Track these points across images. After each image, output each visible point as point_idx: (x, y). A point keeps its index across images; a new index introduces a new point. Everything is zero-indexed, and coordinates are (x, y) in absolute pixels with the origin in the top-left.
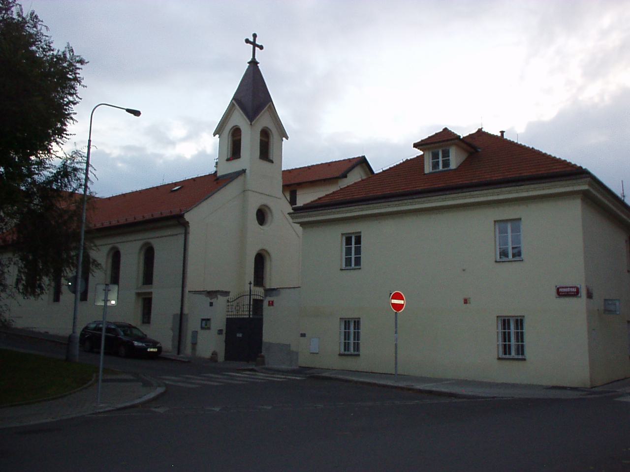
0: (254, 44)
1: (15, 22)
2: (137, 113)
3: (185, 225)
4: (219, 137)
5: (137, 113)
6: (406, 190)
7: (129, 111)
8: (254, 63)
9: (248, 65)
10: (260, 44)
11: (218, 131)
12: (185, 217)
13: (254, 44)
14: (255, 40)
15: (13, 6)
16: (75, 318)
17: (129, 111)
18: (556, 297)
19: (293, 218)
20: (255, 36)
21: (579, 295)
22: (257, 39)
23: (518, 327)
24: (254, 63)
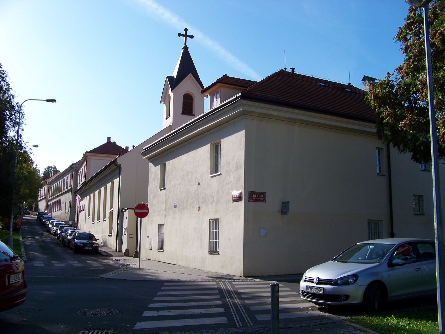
0: (186, 36)
2: (53, 101)
5: (53, 101)
7: (47, 101)
8: (186, 49)
14: (186, 33)
17: (47, 101)
18: (248, 201)
24: (186, 49)
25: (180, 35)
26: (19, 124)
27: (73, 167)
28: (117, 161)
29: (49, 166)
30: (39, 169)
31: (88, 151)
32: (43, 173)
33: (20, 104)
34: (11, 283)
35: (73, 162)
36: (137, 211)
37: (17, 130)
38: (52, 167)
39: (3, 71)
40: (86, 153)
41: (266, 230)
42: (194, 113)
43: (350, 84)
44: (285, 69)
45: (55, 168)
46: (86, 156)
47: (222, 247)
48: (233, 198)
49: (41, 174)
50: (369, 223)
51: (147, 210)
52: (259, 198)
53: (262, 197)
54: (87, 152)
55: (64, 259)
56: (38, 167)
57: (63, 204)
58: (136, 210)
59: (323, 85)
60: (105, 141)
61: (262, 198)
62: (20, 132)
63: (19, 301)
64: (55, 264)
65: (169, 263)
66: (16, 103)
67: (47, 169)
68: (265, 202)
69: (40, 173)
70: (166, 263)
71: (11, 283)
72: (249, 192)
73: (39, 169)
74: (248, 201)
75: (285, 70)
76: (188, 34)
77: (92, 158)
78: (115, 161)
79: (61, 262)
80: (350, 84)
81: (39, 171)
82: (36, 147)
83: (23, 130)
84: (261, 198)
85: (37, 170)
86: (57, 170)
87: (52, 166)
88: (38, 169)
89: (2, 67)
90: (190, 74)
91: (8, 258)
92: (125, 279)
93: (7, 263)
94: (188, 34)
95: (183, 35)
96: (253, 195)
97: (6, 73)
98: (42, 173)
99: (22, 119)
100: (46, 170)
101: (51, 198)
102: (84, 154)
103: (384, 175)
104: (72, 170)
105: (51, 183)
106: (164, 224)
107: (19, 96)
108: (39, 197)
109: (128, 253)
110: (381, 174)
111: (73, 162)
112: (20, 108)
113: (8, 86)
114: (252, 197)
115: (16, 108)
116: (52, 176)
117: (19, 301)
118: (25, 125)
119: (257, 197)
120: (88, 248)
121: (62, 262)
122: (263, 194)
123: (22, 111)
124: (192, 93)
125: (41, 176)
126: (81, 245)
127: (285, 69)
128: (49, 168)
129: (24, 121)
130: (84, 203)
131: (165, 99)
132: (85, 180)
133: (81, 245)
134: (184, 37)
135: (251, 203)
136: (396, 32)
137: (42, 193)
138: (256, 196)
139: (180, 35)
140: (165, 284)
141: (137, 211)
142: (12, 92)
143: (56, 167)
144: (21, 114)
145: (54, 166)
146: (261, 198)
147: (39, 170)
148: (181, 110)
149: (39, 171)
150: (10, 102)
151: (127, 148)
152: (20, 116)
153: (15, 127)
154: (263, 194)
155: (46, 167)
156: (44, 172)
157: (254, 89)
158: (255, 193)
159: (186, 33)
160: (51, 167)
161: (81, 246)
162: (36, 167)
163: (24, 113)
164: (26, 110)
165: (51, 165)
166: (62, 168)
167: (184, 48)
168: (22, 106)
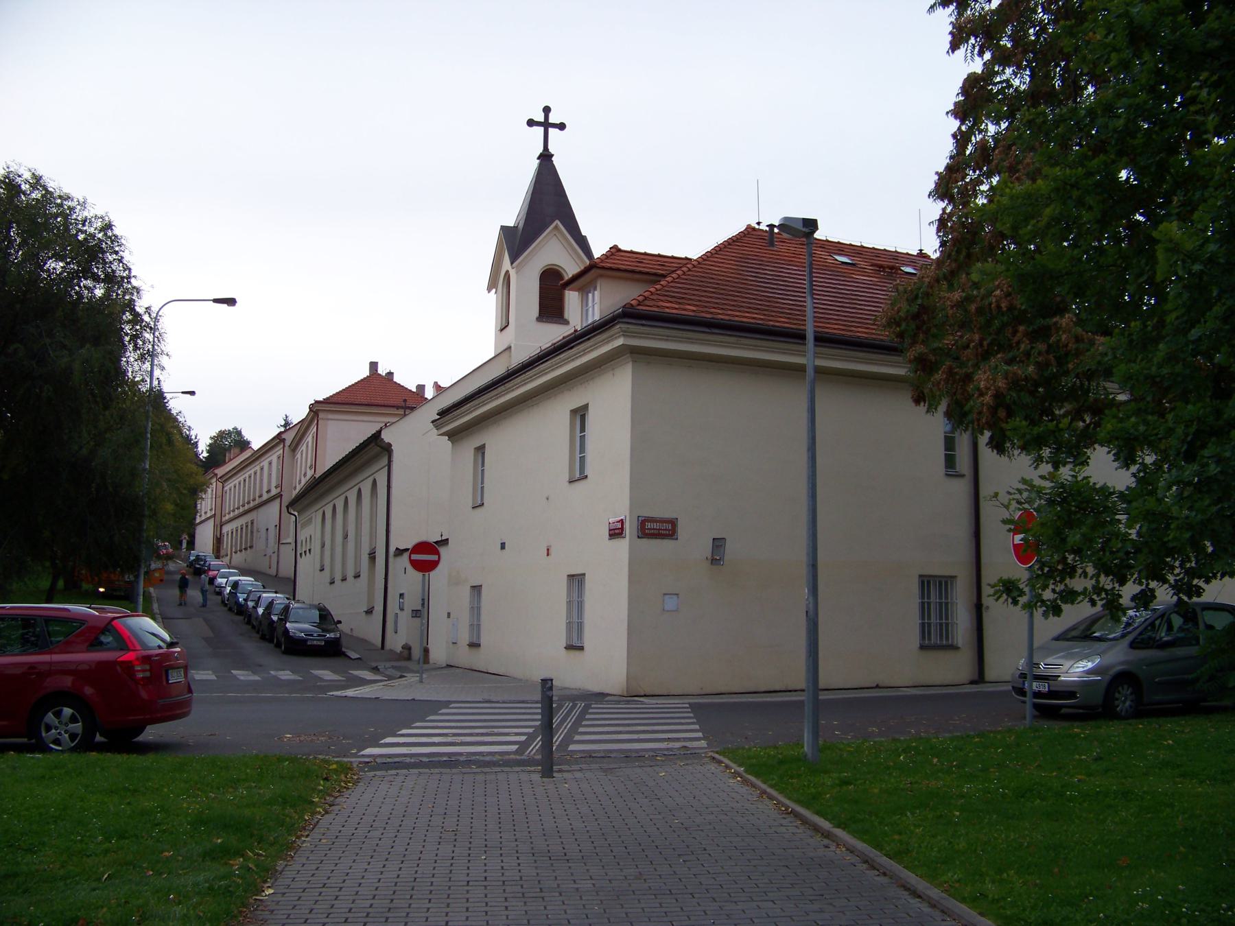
0: (546, 125)
1: (1009, 67)
2: (231, 302)
3: (387, 449)
4: (496, 293)
5: (231, 302)
6: (772, 323)
7: (217, 301)
8: (546, 157)
9: (538, 161)
10: (535, 128)
11: (492, 285)
12: (382, 437)
13: (546, 125)
14: (547, 117)
15: (976, 41)
16: (915, 687)
17: (217, 301)
18: (638, 537)
19: (437, 427)
20: (547, 110)
21: (675, 537)
22: (551, 115)
23: (925, 638)
24: (546, 157)
25: (531, 123)
26: (152, 354)
27: (284, 439)
30: (196, 438)
31: (321, 399)
32: (208, 448)
33: (155, 309)
34: (170, 682)
36: (414, 557)
37: (149, 369)
39: (116, 236)
40: (317, 405)
41: (678, 597)
42: (566, 316)
43: (921, 250)
44: (759, 223)
45: (239, 433)
46: (317, 409)
48: (610, 530)
49: (200, 452)
50: (923, 582)
51: (437, 556)
52: (661, 529)
53: (670, 528)
54: (317, 402)
55: (261, 666)
56: (193, 433)
58: (412, 555)
59: (843, 263)
60: (365, 373)
61: (669, 530)
62: (157, 373)
63: (231, 570)
64: (238, 677)
65: (490, 673)
66: (146, 308)
68: (677, 539)
69: (200, 449)
70: (485, 673)
71: (170, 682)
72: (640, 519)
73: (196, 438)
74: (638, 537)
75: (757, 227)
77: (330, 416)
78: (376, 436)
79: (253, 672)
80: (921, 250)
81: (197, 442)
82: (189, 395)
83: (163, 369)
84: (666, 530)
85: (192, 440)
86: (245, 439)
88: (193, 437)
89: (113, 227)
91: (162, 644)
92: (376, 698)
93: (161, 651)
95: (538, 124)
96: (648, 525)
97: (123, 241)
98: (205, 450)
99: (159, 344)
100: (215, 441)
101: (227, 517)
102: (310, 408)
103: (963, 476)
104: (282, 446)
105: (224, 479)
106: (481, 586)
107: (150, 289)
108: (199, 514)
109: (410, 654)
110: (957, 474)
112: (156, 318)
113: (127, 272)
114: (648, 529)
115: (146, 318)
116: (231, 460)
117: (231, 570)
118: (168, 357)
119: (659, 529)
121: (254, 673)
122: (673, 523)
123: (159, 327)
124: (562, 268)
125: (201, 457)
127: (759, 223)
128: (222, 435)
129: (164, 349)
130: (311, 531)
131: (500, 281)
132: (315, 472)
134: (542, 128)
135: (644, 540)
136: (930, 183)
137: (206, 505)
138: (655, 527)
139: (531, 123)
140: (452, 705)
141: (414, 557)
142: (134, 282)
143: (240, 431)
144: (157, 334)
145: (237, 429)
146: (666, 530)
147: (196, 440)
149: (197, 442)
150: (130, 306)
151: (421, 388)
152: (154, 337)
153: (144, 363)
154: (673, 523)
156: (210, 445)
157: (658, 292)
159: (547, 117)
163: (163, 331)
164: (165, 324)
166: (257, 439)
168: (160, 314)
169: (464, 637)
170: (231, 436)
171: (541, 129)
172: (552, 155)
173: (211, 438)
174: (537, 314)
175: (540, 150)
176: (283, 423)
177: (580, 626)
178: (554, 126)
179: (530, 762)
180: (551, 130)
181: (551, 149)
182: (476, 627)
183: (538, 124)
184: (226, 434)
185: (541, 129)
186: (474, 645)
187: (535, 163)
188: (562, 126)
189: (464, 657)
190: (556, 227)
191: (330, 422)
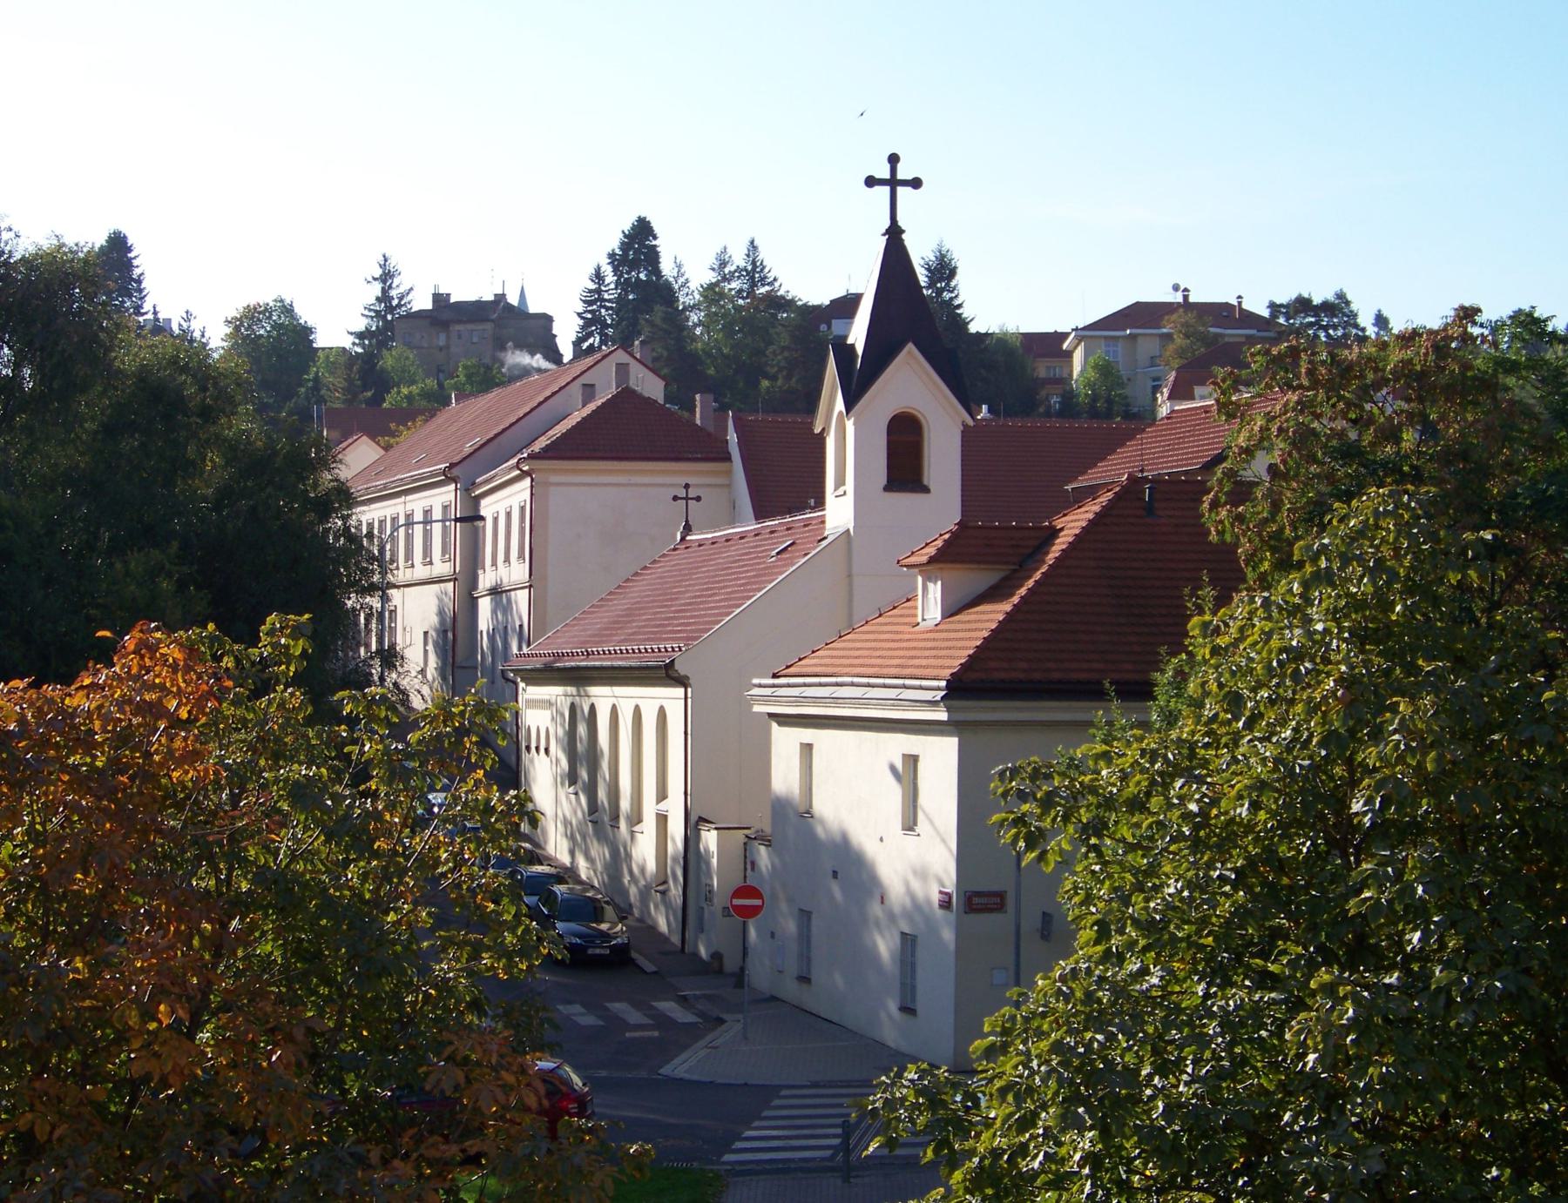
8: (894, 233)
10: (877, 188)
13: (893, 183)
14: (893, 171)
24: (894, 233)
25: (871, 182)
28: (677, 666)
29: (252, 303)
30: (203, 336)
35: (386, 260)
38: (267, 311)
42: (925, 482)
45: (288, 310)
47: (922, 1002)
57: (408, 635)
67: (240, 319)
73: (203, 336)
76: (902, 174)
77: (554, 479)
86: (302, 321)
87: (271, 304)
88: (197, 335)
90: (910, 347)
94: (902, 174)
95: (882, 182)
96: (976, 900)
111: (386, 260)
120: (598, 951)
126: (579, 941)
133: (579, 941)
139: (871, 182)
140: (784, 1093)
145: (282, 301)
148: (882, 479)
155: (234, 310)
158: (979, 894)
159: (893, 171)
160: (266, 309)
161: (576, 944)
162: (185, 325)
165: (265, 296)
167: (888, 232)
169: (792, 968)
170: (270, 317)
171: (886, 189)
172: (903, 231)
173: (228, 322)
174: (883, 480)
175: (887, 223)
176: (378, 272)
177: (913, 988)
178: (905, 183)
179: (832, 1169)
180: (900, 190)
181: (901, 222)
182: (806, 958)
183: (882, 182)
184: (259, 313)
185: (886, 189)
186: (804, 979)
187: (882, 242)
188: (916, 183)
189: (790, 989)
190: (909, 352)
191: (552, 489)
